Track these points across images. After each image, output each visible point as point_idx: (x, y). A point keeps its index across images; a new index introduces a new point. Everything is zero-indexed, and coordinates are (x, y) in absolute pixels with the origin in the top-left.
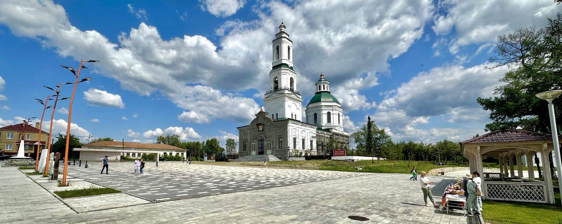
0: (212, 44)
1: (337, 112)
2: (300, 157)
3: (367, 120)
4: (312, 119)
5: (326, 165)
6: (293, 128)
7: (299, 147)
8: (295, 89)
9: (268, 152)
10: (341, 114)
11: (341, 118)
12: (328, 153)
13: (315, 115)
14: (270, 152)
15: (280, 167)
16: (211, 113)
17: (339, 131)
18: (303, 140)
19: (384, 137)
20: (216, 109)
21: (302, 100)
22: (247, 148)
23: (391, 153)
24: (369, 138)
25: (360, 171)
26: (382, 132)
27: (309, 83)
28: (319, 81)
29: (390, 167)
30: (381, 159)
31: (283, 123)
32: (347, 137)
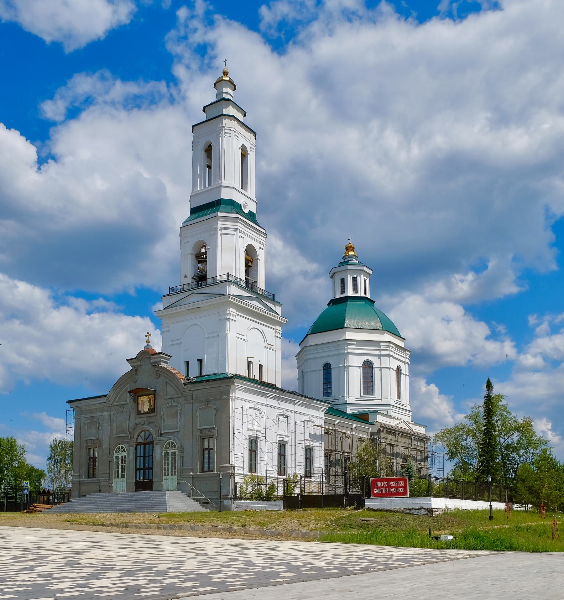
0: (23, 139)
1: (394, 364)
2: (268, 497)
3: (484, 391)
4: (318, 378)
5: (343, 526)
6: (247, 405)
7: (268, 468)
8: (261, 284)
9: (165, 484)
10: (405, 369)
11: (405, 381)
12: (356, 489)
13: (327, 368)
14: (174, 484)
15: (194, 531)
16: (14, 358)
17: (399, 419)
18: (282, 447)
19: (529, 443)
20: (33, 349)
21: (284, 320)
22: (100, 468)
23: (545, 491)
24: (488, 445)
25: (449, 546)
26: (525, 429)
27: (317, 276)
28: (341, 264)
29: (539, 533)
30: (516, 507)
31: (214, 388)
32: (422, 439)
